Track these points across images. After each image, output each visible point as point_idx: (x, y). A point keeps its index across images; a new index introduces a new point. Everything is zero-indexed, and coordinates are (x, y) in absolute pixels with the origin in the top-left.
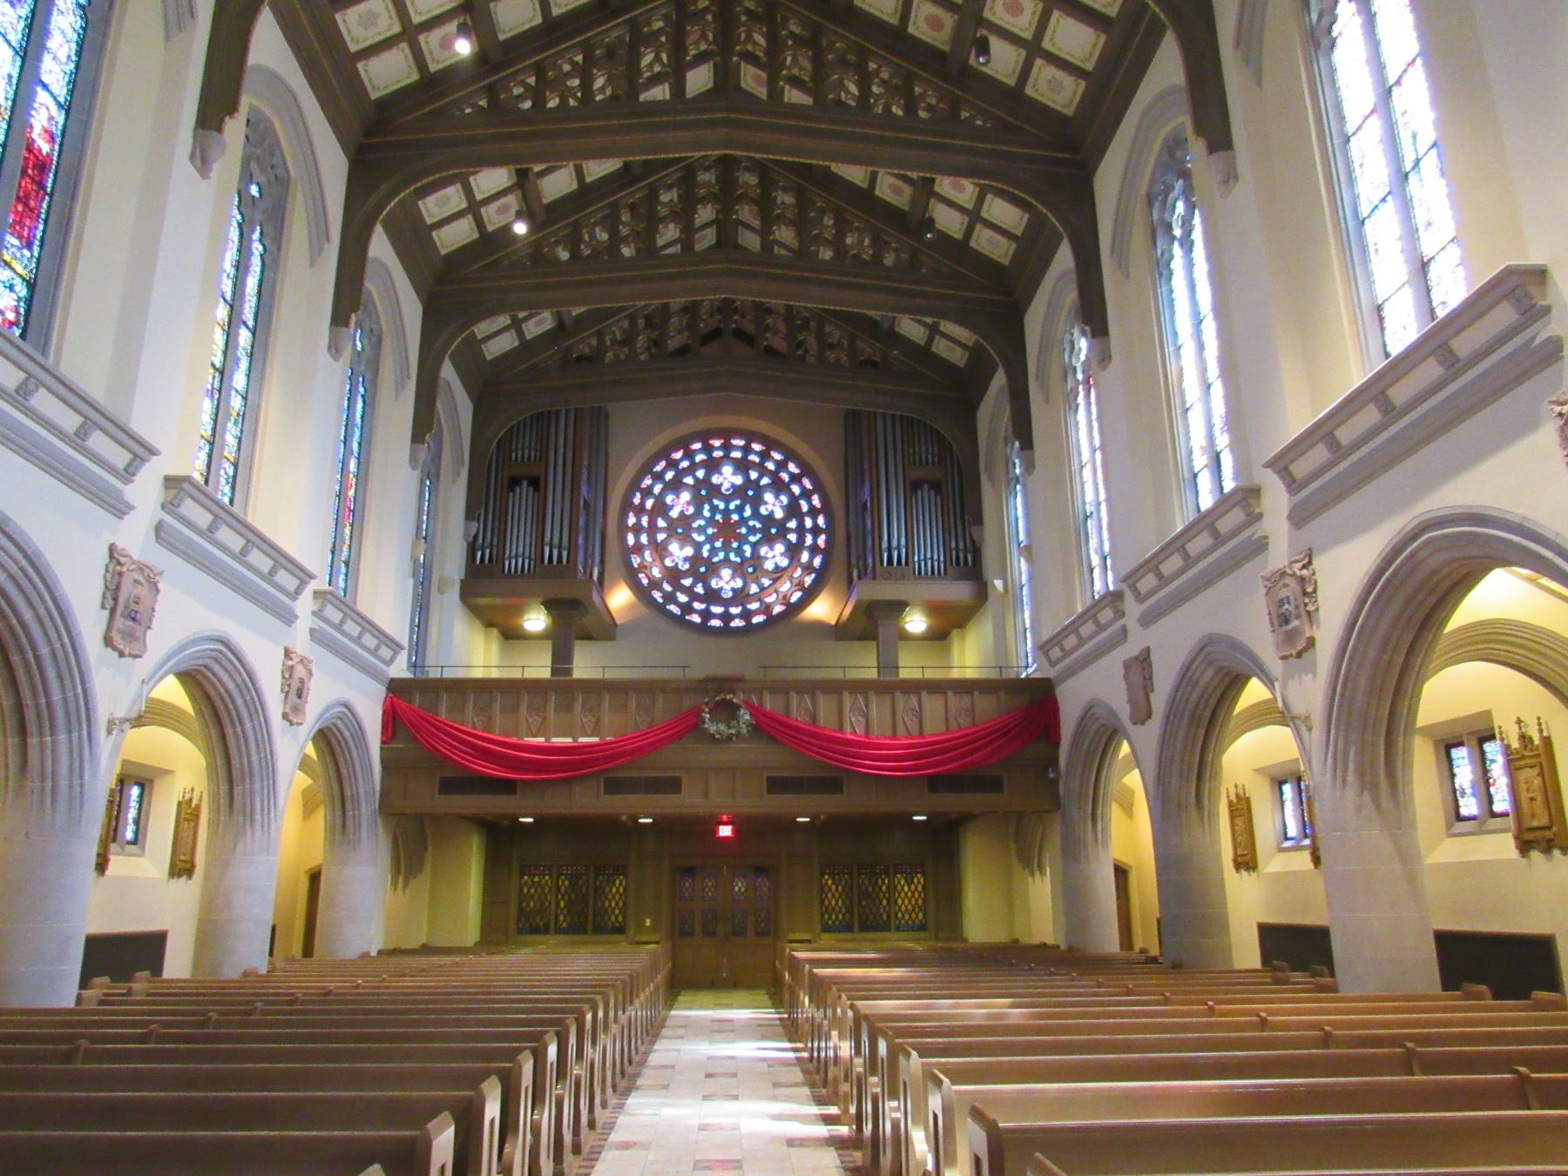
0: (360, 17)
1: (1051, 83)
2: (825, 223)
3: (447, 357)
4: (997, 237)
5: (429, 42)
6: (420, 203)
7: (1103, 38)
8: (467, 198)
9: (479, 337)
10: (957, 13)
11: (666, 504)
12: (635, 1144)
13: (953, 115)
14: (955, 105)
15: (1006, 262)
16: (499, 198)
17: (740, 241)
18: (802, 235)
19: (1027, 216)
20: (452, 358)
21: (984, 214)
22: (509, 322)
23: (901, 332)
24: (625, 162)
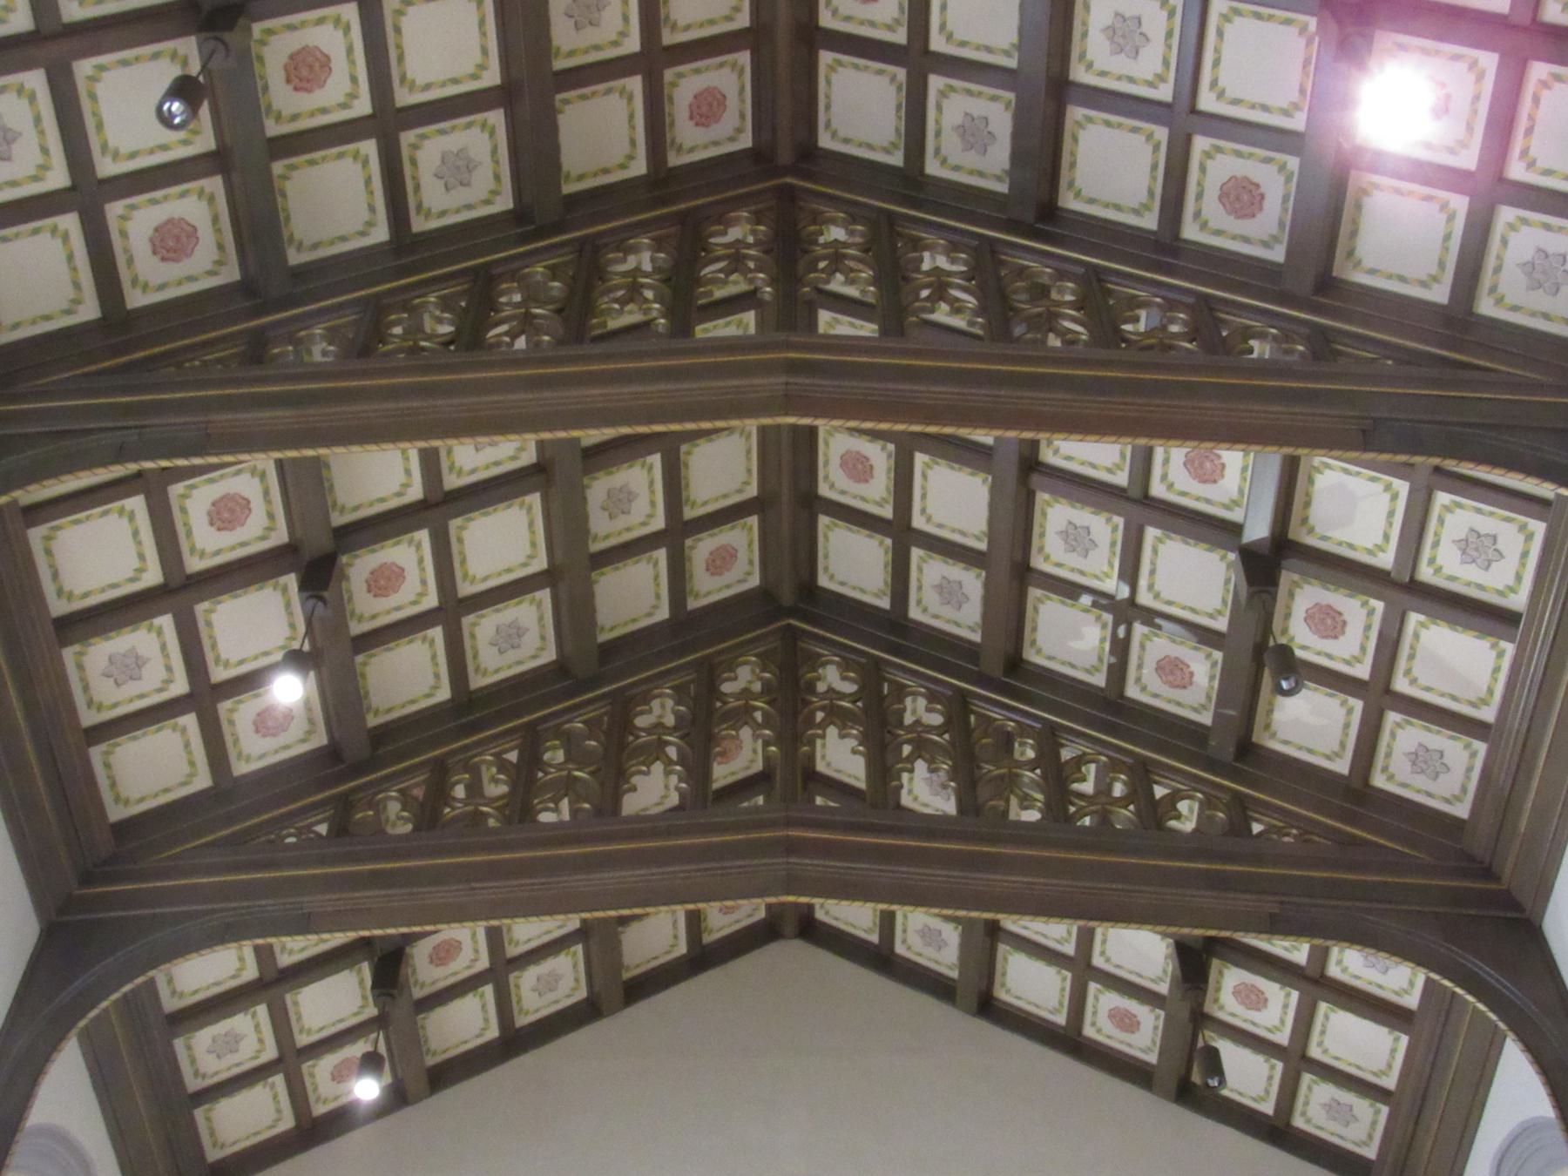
0: (214, 1040)
1: (1332, 1108)
2: (1017, 755)
3: (74, 1031)
4: (1348, 1097)
5: (320, 1071)
6: (179, 1044)
7: (1404, 1040)
8: (217, 719)
9: (170, 1004)
10: (1161, 1007)
11: (542, 759)
12: (1432, 689)
13: (1239, 827)
14: (1241, 809)
15: (1462, 811)
16: (341, 1046)
17: (821, 767)
18: (967, 781)
19: (1404, 1040)
20: (87, 1041)
21: (1401, 685)
22: (251, 972)
23: (1274, 745)
24: (584, 921)
